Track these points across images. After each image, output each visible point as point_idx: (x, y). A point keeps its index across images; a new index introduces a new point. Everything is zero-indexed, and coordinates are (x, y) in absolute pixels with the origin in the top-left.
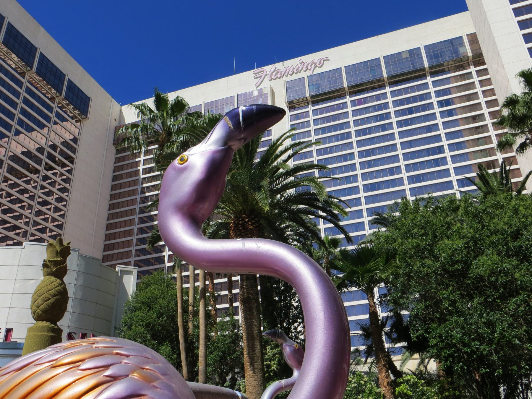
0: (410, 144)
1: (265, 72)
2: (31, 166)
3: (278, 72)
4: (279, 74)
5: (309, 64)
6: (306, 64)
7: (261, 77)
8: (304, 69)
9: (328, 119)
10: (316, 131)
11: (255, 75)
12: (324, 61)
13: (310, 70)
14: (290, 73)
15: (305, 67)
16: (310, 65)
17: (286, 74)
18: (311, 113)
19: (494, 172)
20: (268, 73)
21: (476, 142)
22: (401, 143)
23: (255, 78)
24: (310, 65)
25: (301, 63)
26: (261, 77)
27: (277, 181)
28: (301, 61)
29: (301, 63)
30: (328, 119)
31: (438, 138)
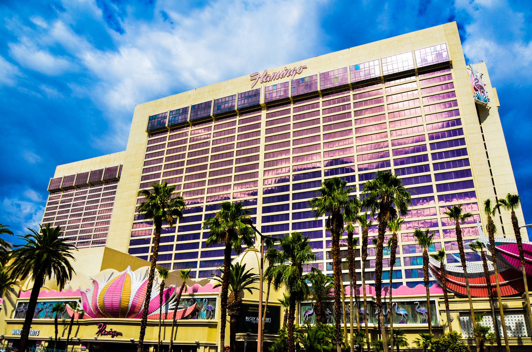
0: (442, 166)
1: (259, 75)
2: (340, 179)
3: (268, 77)
4: (269, 78)
5: (291, 71)
6: (289, 71)
7: (256, 79)
8: (288, 75)
9: (335, 117)
10: (134, 225)
11: (252, 78)
12: (303, 68)
13: (291, 75)
14: (277, 78)
15: (288, 73)
16: (292, 71)
17: (274, 79)
18: (321, 104)
19: (269, 259)
20: (261, 76)
21: (455, 164)
22: (434, 164)
23: (251, 80)
24: (292, 71)
25: (285, 70)
26: (256, 79)
27: (72, 336)
28: (286, 69)
29: (285, 70)
30: (335, 117)
31: (425, 158)
